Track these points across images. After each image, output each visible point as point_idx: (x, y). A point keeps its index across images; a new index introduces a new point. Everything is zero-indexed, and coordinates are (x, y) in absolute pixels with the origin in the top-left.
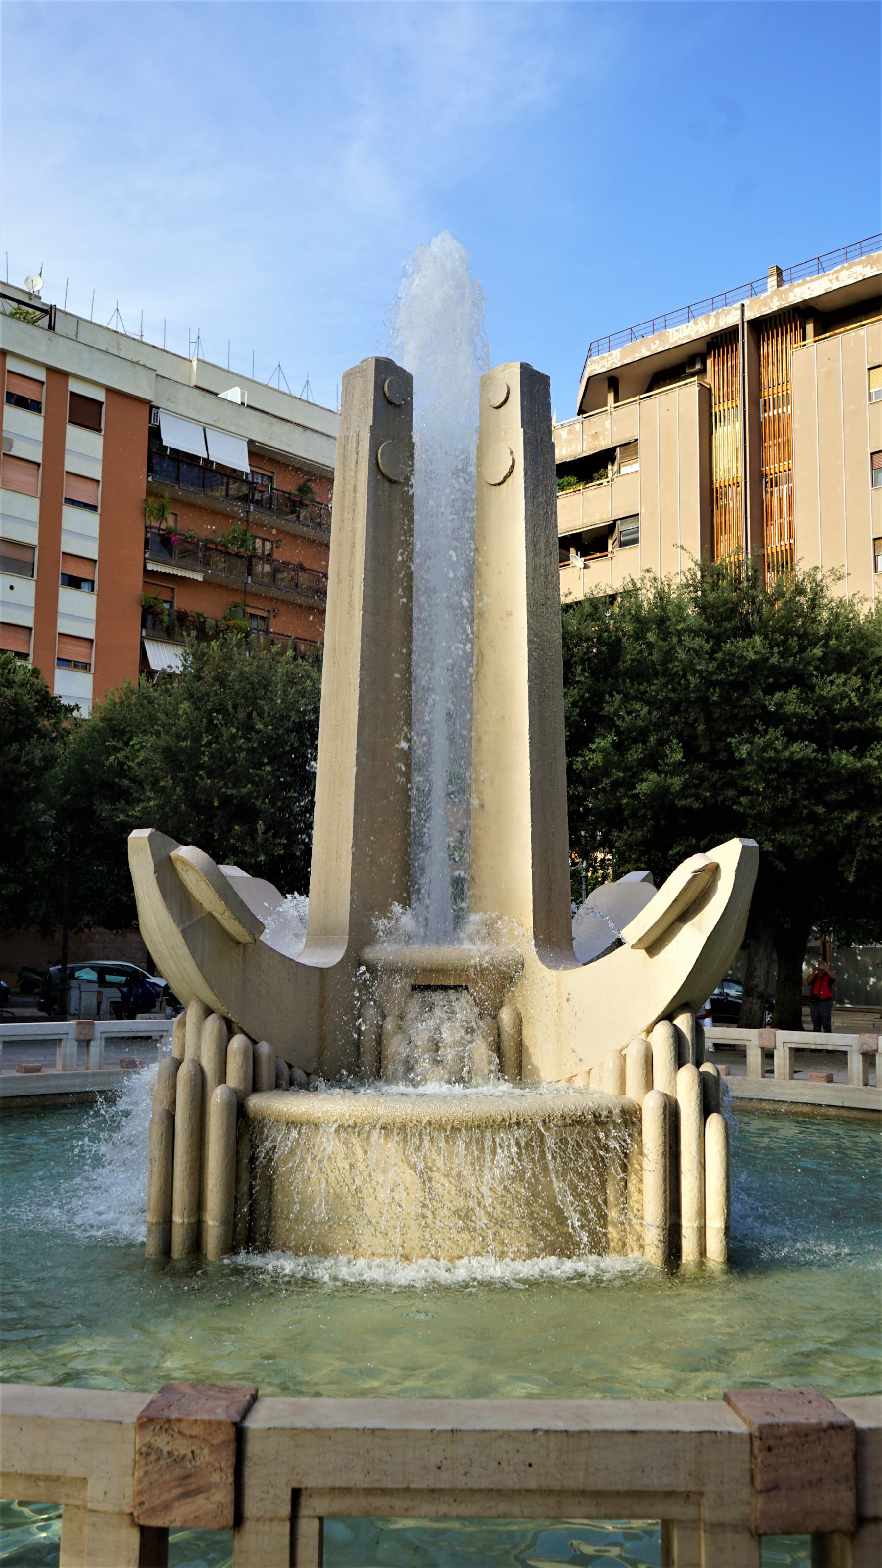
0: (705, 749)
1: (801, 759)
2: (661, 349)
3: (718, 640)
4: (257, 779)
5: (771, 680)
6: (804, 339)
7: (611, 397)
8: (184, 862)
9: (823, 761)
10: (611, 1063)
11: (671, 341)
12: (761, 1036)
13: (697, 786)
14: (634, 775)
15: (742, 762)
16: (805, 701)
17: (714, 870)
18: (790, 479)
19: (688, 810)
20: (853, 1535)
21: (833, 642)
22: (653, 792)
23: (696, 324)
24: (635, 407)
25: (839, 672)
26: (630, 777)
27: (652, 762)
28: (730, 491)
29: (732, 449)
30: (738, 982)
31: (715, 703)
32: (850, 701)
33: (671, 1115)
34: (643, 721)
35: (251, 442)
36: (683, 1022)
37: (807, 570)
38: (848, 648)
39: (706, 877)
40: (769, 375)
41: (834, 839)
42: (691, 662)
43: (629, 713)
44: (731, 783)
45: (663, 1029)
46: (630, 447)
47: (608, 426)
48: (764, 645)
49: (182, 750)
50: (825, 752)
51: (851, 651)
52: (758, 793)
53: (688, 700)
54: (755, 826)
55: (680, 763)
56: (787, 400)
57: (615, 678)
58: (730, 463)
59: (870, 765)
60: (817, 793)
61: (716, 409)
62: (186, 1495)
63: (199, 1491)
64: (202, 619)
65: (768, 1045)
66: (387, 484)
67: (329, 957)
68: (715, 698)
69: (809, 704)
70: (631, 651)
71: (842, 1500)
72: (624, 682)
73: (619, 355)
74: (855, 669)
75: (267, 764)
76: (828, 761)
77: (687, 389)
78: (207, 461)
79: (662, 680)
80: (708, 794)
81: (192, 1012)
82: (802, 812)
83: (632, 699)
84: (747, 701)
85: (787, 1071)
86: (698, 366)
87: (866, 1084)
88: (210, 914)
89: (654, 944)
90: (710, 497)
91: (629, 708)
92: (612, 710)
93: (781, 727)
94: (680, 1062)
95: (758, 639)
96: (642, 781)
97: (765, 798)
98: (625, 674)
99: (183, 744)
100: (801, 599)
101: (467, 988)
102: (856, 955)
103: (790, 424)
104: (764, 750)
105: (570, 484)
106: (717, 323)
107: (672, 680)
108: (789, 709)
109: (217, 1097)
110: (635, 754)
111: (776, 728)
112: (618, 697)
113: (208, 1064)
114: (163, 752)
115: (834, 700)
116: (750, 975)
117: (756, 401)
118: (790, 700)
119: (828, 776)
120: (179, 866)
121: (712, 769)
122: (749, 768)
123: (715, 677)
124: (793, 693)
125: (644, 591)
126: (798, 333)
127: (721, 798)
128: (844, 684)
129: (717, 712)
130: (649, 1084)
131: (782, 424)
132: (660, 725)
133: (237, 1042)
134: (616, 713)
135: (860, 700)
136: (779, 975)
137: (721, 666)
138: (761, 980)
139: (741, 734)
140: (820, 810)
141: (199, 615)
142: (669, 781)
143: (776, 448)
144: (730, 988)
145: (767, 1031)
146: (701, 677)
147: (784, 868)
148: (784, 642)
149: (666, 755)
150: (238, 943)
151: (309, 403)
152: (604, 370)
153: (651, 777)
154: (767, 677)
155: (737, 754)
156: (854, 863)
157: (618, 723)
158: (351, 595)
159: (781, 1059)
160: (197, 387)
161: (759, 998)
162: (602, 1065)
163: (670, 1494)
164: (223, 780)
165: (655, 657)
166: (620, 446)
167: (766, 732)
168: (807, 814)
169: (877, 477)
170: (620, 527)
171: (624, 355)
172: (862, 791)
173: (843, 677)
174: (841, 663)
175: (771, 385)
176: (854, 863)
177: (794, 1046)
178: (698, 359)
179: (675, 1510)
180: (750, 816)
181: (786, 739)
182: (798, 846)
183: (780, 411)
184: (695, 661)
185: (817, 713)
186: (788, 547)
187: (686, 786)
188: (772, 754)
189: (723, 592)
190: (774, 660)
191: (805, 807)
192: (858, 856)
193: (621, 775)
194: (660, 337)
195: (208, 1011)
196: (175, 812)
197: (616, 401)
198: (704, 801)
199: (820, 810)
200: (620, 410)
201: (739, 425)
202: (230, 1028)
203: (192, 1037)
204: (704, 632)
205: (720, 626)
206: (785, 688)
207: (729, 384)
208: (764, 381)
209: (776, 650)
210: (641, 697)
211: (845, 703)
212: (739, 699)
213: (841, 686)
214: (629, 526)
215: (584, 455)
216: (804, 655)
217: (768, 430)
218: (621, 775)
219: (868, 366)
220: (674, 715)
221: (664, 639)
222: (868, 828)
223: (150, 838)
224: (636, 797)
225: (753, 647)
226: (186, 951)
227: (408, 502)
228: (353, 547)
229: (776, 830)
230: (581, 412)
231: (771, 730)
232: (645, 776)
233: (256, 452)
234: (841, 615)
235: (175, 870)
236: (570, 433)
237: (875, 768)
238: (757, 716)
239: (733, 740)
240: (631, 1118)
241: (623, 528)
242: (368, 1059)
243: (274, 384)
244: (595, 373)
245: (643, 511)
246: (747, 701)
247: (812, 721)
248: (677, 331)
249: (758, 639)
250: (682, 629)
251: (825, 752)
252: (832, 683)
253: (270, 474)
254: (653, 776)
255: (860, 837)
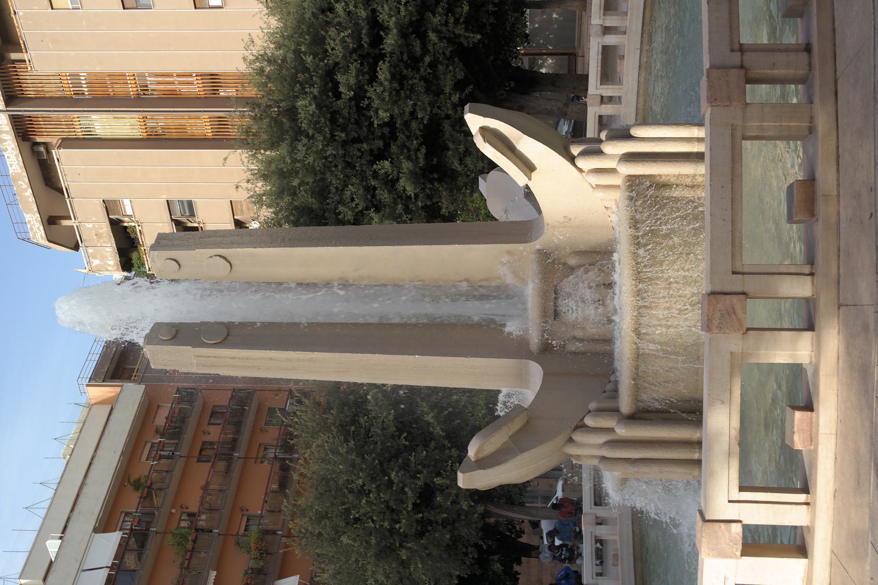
0: (380, 144)
1: (390, 72)
2: (26, 180)
3: (298, 133)
4: (401, 485)
5: (330, 94)
6: (25, 61)
7: (65, 223)
8: (478, 452)
9: (391, 57)
10: (600, 194)
11: (20, 171)
12: (592, 105)
13: (409, 150)
14: (400, 197)
15: (392, 117)
16: (347, 69)
17: (484, 130)
18: (142, 75)
19: (427, 155)
20: (746, 70)
21: (303, 49)
22: (414, 183)
23: (6, 150)
24: (76, 201)
25: (324, 43)
26: (402, 199)
27: (391, 183)
28: (150, 124)
29: (114, 122)
30: (557, 124)
31: (347, 135)
32: (348, 36)
33: (631, 157)
34: (359, 189)
35: (96, 530)
36: (575, 150)
37: (245, 66)
38: (307, 37)
39: (488, 135)
40: (52, 90)
41: (449, 50)
42: (317, 152)
43: (353, 200)
44: (407, 124)
45: (580, 163)
46: (109, 206)
47: (90, 225)
48: (304, 98)
49: (378, 544)
50: (385, 55)
51: (309, 35)
52: (415, 105)
53: (344, 156)
54: (439, 108)
55: (391, 162)
56: (75, 76)
57: (324, 211)
58: (125, 124)
59: (395, 23)
60: (414, 62)
61: (80, 135)
62: (734, 313)
63: (733, 308)
64: (250, 571)
65: (599, 31)
66: (230, 338)
67: (536, 371)
68: (343, 135)
69: (348, 67)
70: (305, 198)
71: (734, 73)
72: (328, 204)
73: (29, 215)
74: (322, 32)
75: (389, 477)
76: (392, 53)
77: (62, 159)
78: (111, 568)
79: (328, 175)
80: (415, 142)
81: (572, 450)
82: (429, 73)
83: (341, 199)
84: (345, 112)
85: (617, 87)
86: (42, 149)
87: (625, 33)
88: (510, 437)
89: (528, 167)
90: (154, 140)
91: (349, 200)
92: (350, 213)
93: (366, 87)
94: (600, 153)
95: (300, 103)
96: (405, 190)
97: (418, 100)
98: (321, 203)
99: (373, 542)
100: (268, 69)
101: (555, 286)
102: (534, 28)
103: (96, 74)
104: (383, 100)
105: (139, 258)
106: (6, 132)
107: (328, 167)
108: (352, 81)
109: (623, 432)
110: (384, 195)
111: (366, 91)
112: (341, 208)
113: (601, 439)
114: (378, 560)
115: (345, 48)
116: (550, 113)
117: (75, 101)
118: (346, 80)
119: (402, 53)
120: (481, 455)
121: (395, 138)
122: (396, 111)
123: (328, 136)
124: (340, 77)
125: (257, 189)
126: (17, 66)
127: (418, 133)
128: (334, 40)
129: (354, 134)
130: (613, 171)
131: (95, 80)
132: (363, 178)
133: (589, 421)
134: (352, 209)
135: (346, 29)
136: (551, 91)
137: (319, 131)
138: (558, 107)
139: (371, 117)
140: (427, 59)
141: (246, 573)
142: (405, 170)
143: (115, 86)
144: (562, 130)
145: (588, 100)
146: (327, 145)
147: (471, 87)
148: (301, 84)
149: (386, 173)
150: (528, 422)
151: (59, 483)
152: (42, 228)
153: (403, 184)
154: (328, 97)
155: (386, 120)
156: (467, 34)
157: (360, 208)
158: (303, 360)
159: (608, 91)
160: (45, 579)
161: (567, 106)
162: (602, 200)
163: (733, 136)
164: (401, 512)
165: (310, 180)
166: (108, 215)
167: (369, 98)
168: (431, 69)
169: (144, 5)
170: (177, 216)
171: (30, 211)
172: (414, 29)
173: (328, 40)
174: (318, 41)
175: (61, 89)
176: (467, 34)
177: (599, 82)
178: (36, 148)
179: (739, 134)
180: (432, 111)
181: (374, 84)
182: (454, 76)
183: (84, 82)
184: (315, 149)
185: (356, 61)
186: (199, 78)
187: (409, 158)
188: (386, 94)
189: (262, 128)
190: (316, 91)
191: (425, 70)
192: (462, 32)
193: (400, 206)
194: (16, 180)
195: (571, 440)
196: (426, 548)
197: (69, 218)
198: (420, 145)
199: (427, 59)
200: (78, 214)
201: (94, 116)
202: (580, 426)
203: (587, 449)
204: (292, 143)
205: (287, 132)
206: (337, 84)
207: (58, 122)
208: (59, 94)
209: (307, 90)
210: (341, 191)
211: (348, 40)
212: (344, 118)
213: (337, 44)
214: (177, 209)
215: (114, 245)
216: (312, 70)
217: (99, 91)
218: (400, 206)
219: (50, 10)
220: (355, 167)
221: (297, 173)
222: (442, 25)
223: (463, 472)
224: (416, 195)
225: (306, 107)
226: (533, 451)
227: (242, 325)
228: (272, 359)
229: (442, 92)
230: (76, 248)
231: (368, 95)
232: (401, 188)
233: (104, 526)
234: (280, 40)
235: (483, 459)
236: (95, 257)
237: (397, 19)
238: (357, 105)
239: (376, 122)
240: (633, 181)
241: (179, 214)
242: (599, 348)
243: (43, 513)
244: (44, 235)
245: (165, 197)
246: (345, 112)
247: (362, 64)
248: (11, 166)
249: (300, 103)
250: (290, 159)
251: (385, 55)
252: (333, 49)
253: (123, 515)
254: (402, 182)
255: (448, 30)
